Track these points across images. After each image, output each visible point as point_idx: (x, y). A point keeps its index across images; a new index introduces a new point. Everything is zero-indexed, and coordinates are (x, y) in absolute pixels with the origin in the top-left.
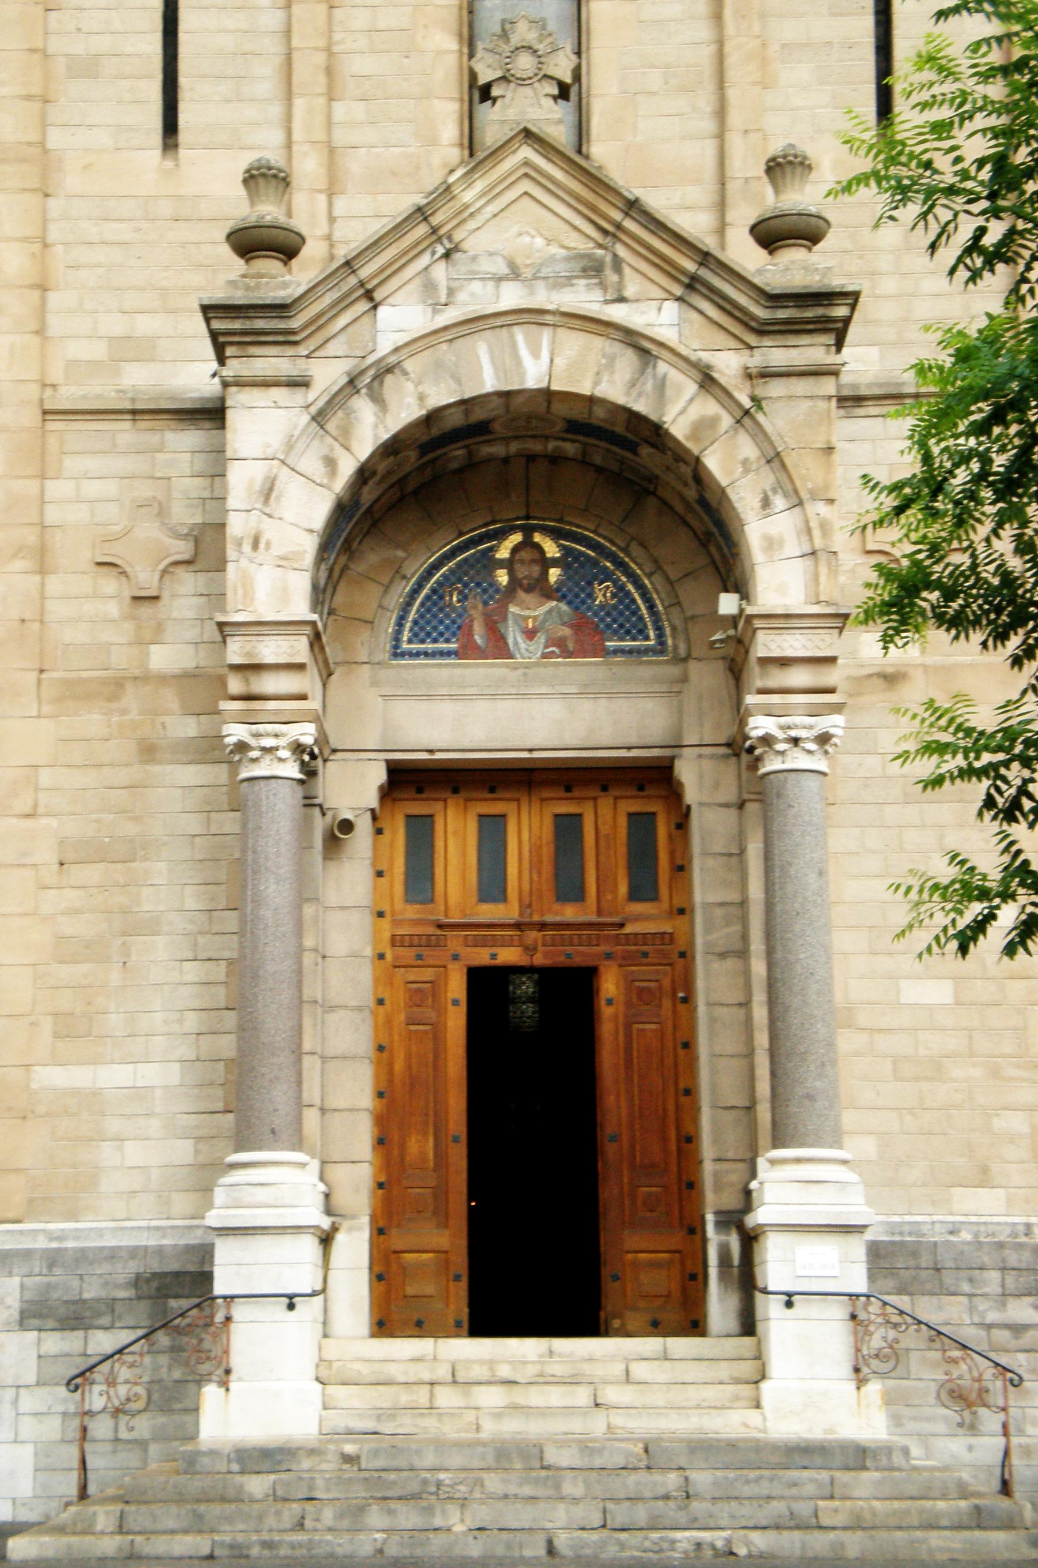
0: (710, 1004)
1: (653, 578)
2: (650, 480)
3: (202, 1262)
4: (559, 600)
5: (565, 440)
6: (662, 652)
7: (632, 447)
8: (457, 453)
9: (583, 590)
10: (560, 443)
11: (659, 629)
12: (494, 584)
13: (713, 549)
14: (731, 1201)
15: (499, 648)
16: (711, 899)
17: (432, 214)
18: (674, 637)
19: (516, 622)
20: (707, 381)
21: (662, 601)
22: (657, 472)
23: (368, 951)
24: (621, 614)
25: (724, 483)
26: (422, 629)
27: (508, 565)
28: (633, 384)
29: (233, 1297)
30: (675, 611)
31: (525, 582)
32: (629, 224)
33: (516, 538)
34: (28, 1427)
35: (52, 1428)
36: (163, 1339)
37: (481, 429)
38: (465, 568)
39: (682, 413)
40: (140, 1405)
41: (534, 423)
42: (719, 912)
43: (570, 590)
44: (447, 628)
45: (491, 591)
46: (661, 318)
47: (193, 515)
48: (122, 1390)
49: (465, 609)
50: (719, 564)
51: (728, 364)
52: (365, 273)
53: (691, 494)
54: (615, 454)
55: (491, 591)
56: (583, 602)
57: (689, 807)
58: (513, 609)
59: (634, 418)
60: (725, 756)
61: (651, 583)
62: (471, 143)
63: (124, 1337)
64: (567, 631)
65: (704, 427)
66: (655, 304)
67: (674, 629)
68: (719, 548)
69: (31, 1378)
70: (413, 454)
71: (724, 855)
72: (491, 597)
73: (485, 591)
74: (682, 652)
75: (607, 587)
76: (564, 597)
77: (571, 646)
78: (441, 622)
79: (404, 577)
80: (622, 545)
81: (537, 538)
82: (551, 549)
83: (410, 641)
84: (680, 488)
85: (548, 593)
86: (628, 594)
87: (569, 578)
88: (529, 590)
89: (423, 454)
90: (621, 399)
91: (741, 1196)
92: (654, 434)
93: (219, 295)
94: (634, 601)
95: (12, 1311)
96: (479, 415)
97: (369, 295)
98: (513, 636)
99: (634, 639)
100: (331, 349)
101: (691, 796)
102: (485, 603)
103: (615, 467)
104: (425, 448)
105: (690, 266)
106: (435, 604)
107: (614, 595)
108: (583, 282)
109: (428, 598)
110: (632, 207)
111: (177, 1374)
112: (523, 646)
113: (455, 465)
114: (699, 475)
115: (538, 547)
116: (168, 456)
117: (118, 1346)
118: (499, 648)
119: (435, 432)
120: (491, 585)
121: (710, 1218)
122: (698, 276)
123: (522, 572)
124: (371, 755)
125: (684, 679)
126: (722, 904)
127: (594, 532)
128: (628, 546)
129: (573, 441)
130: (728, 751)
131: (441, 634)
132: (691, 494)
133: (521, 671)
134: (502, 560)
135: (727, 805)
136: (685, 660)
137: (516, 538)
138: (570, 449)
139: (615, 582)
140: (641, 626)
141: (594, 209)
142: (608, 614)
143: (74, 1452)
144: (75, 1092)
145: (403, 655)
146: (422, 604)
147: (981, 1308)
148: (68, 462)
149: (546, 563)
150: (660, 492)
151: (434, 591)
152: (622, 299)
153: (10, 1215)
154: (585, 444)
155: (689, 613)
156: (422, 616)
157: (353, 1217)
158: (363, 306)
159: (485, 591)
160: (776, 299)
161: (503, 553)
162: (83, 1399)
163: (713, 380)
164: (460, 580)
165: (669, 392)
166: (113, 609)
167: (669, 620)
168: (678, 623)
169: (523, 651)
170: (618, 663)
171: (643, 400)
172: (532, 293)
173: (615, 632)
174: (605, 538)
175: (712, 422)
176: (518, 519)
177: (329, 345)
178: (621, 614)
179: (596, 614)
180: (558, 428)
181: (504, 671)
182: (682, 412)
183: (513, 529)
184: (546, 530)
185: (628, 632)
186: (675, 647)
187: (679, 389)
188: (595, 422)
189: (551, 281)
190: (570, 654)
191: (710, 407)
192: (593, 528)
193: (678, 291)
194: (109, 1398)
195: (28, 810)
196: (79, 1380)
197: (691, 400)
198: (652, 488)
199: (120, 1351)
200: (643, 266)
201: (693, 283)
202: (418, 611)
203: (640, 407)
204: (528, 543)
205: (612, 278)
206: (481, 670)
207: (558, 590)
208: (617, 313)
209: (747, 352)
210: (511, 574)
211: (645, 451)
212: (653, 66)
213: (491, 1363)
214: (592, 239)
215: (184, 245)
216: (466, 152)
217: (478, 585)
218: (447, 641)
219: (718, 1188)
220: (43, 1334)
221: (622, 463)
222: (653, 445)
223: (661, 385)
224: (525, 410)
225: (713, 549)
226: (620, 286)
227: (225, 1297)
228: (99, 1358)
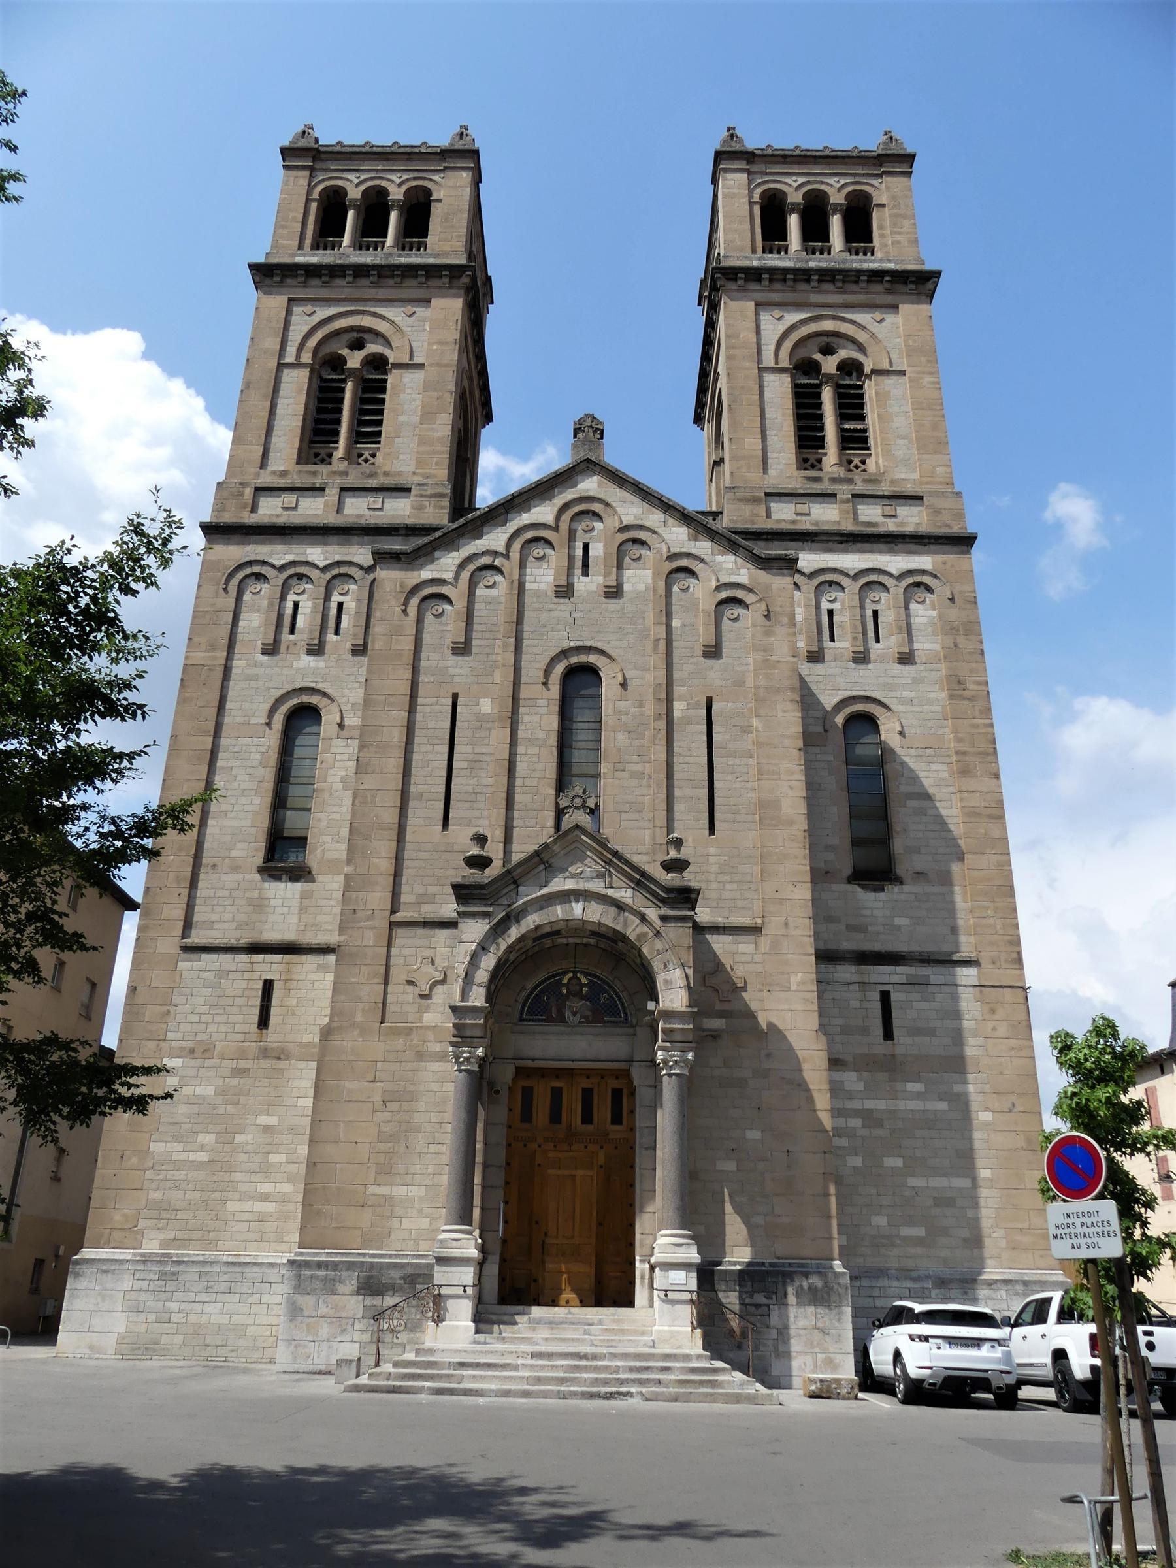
7: (616, 942)
8: (548, 942)
11: (625, 1014)
12: (561, 993)
14: (647, 1251)
20: (643, 918)
27: (567, 985)
28: (615, 919)
33: (571, 975)
35: (367, 1337)
37: (557, 933)
39: (633, 929)
40: (401, 1328)
46: (626, 894)
51: (652, 914)
52: (514, 874)
62: (557, 827)
64: (589, 1013)
69: (360, 1315)
74: (634, 1022)
82: (584, 980)
85: (582, 997)
90: (611, 925)
92: (624, 939)
93: (459, 880)
96: (556, 928)
100: (500, 901)
110: (616, 854)
114: (640, 954)
118: (562, 1019)
119: (539, 934)
121: (637, 1258)
122: (641, 880)
132: (638, 961)
138: (592, 941)
158: (512, 886)
161: (565, 981)
163: (646, 920)
175: (645, 935)
183: (569, 972)
184: (581, 972)
187: (633, 922)
191: (644, 929)
203: (618, 928)
204: (575, 977)
208: (610, 892)
211: (620, 944)
213: (366, 739)
226: (611, 882)
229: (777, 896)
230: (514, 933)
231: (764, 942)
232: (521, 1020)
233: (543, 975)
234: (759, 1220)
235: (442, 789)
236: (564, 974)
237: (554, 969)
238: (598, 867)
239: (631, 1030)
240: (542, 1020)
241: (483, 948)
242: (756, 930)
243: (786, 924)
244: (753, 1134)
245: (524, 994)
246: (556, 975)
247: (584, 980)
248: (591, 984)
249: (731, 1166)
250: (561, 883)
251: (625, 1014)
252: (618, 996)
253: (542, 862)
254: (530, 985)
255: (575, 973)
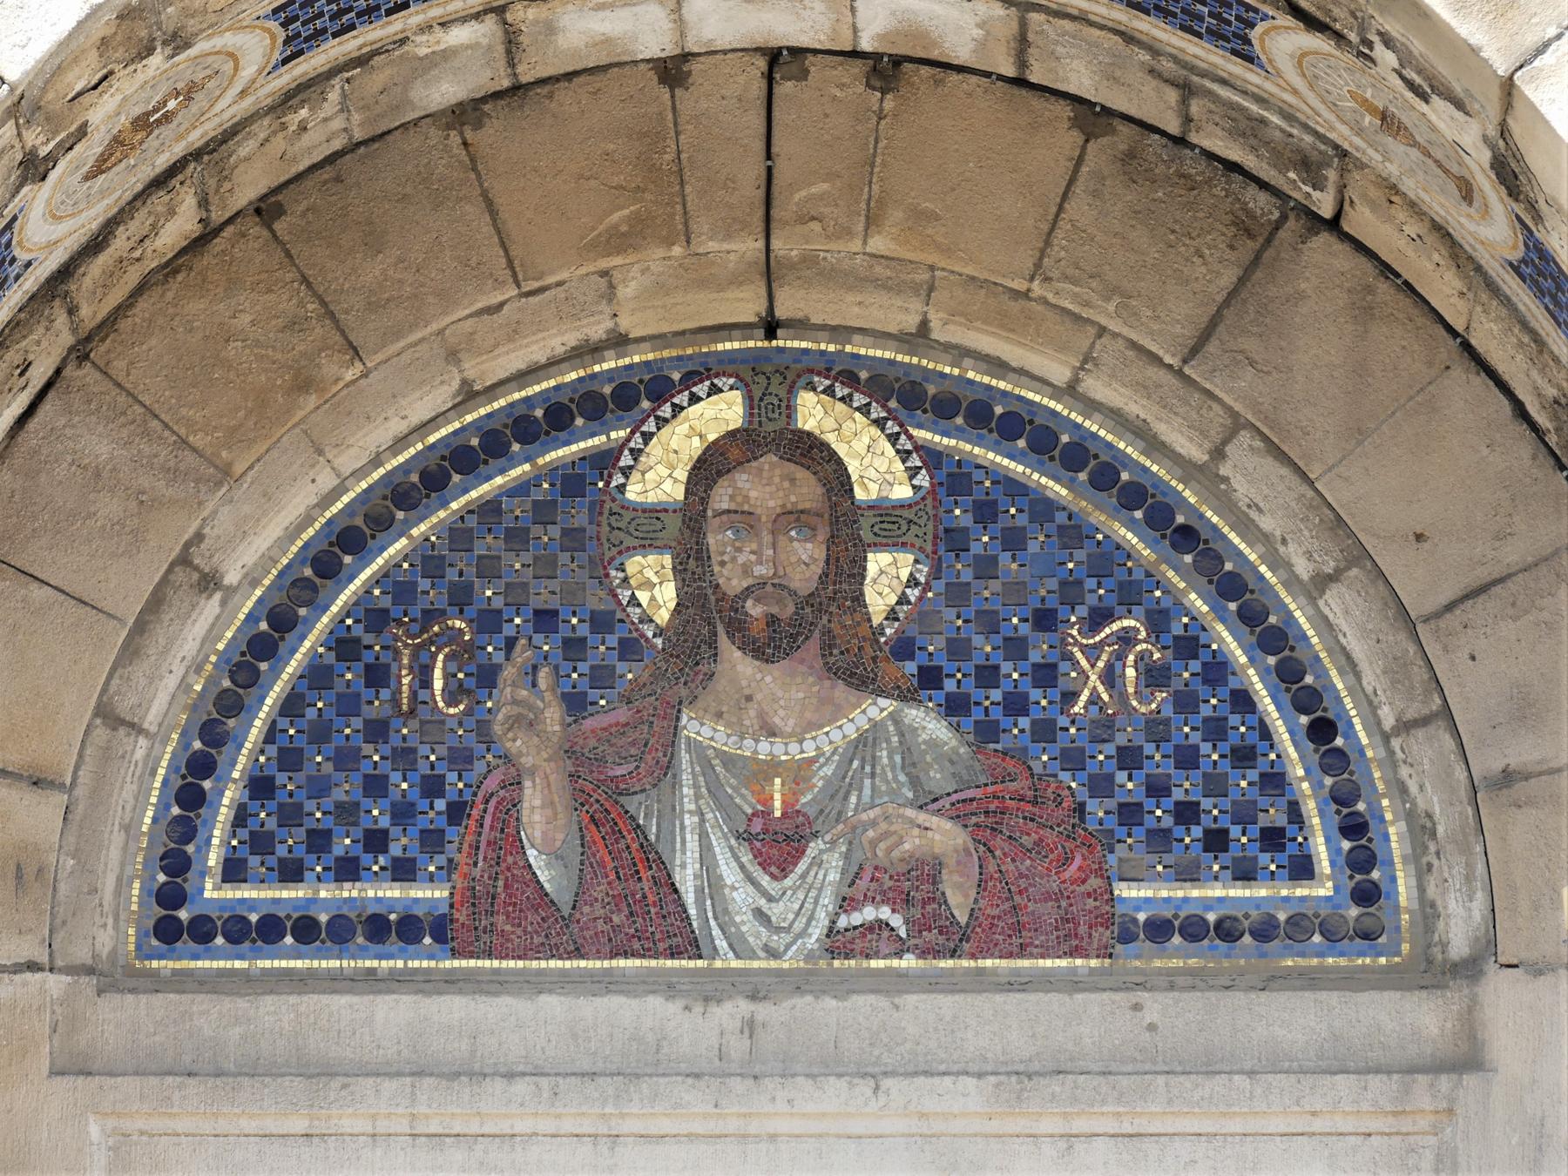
27: (686, 531)
33: (722, 412)
64: (944, 836)
74: (1459, 929)
85: (857, 663)
118: (640, 914)
132: (1491, 232)
161: (659, 479)
183: (701, 375)
184: (845, 377)
204: (770, 437)
232: (174, 923)
233: (396, 416)
236: (651, 394)
237: (528, 351)
239: (1423, 1018)
240: (404, 929)
245: (203, 633)
246: (558, 417)
247: (876, 467)
248: (958, 509)
251: (1362, 860)
252: (1273, 639)
254: (258, 540)
255: (770, 382)
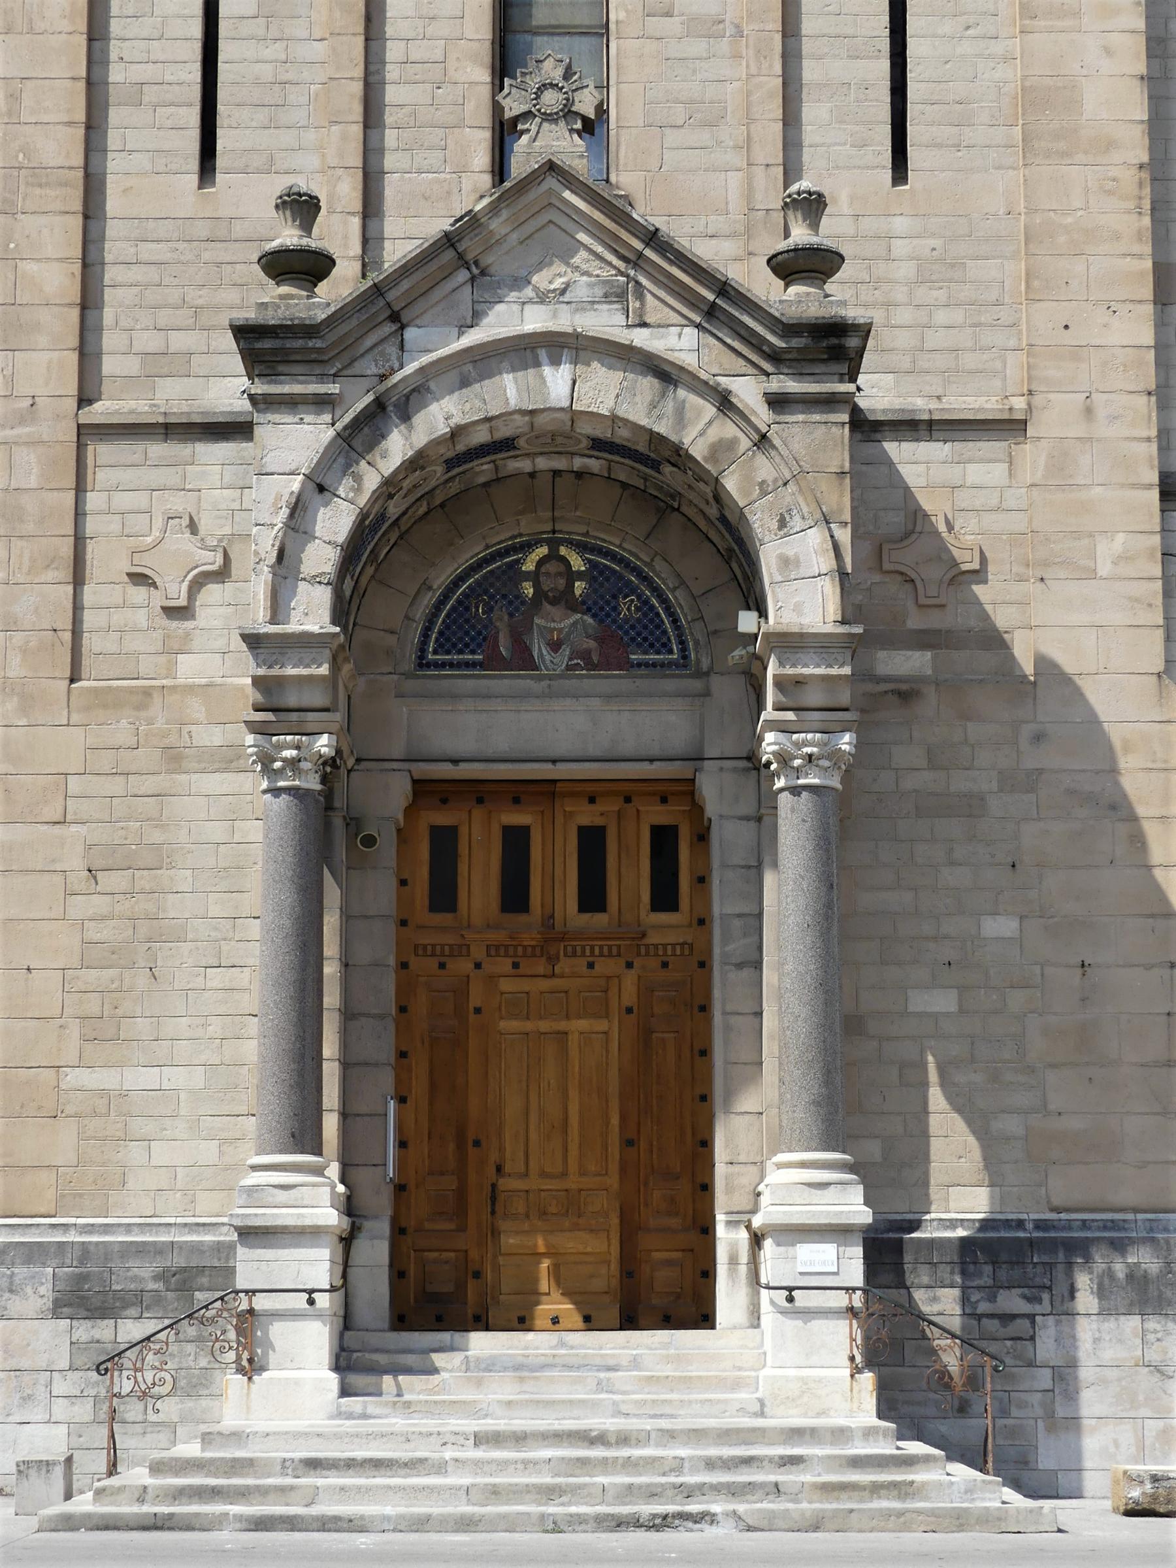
0: (725, 1013)
1: (677, 593)
2: (673, 497)
3: (227, 1259)
4: (583, 614)
5: (591, 457)
6: (685, 666)
7: (655, 465)
8: (483, 469)
9: (608, 603)
10: (587, 460)
13: (735, 566)
14: (745, 1203)
15: (524, 660)
16: (729, 910)
17: (458, 241)
18: (697, 652)
19: (541, 634)
21: (685, 616)
22: (679, 489)
23: (392, 961)
24: (645, 627)
25: (741, 504)
26: (448, 640)
27: (535, 577)
28: (653, 406)
29: (254, 1292)
30: (698, 625)
31: (550, 594)
32: (648, 253)
33: (543, 551)
34: (60, 1409)
35: (83, 1411)
36: (191, 1331)
37: (506, 445)
38: (492, 580)
39: (699, 431)
41: (559, 440)
42: (737, 923)
43: (595, 603)
44: (473, 639)
45: (517, 603)
46: (680, 342)
47: (222, 526)
48: (149, 1376)
49: (490, 620)
50: (741, 581)
52: (391, 296)
53: (713, 512)
54: (639, 471)
55: (517, 603)
56: (608, 615)
57: (710, 820)
58: (537, 621)
59: (655, 438)
60: (746, 770)
61: (676, 598)
62: (499, 169)
63: (150, 1326)
64: (592, 644)
65: (723, 448)
66: (677, 329)
67: (697, 643)
68: (741, 566)
69: (64, 1364)
70: (439, 469)
71: (743, 867)
72: (517, 609)
73: (510, 603)
74: (705, 664)
75: (632, 601)
76: (589, 609)
77: (595, 659)
78: (467, 633)
79: (430, 588)
80: (647, 560)
81: (563, 551)
83: (435, 652)
84: (703, 506)
86: (652, 607)
87: (595, 591)
88: (554, 602)
89: (449, 470)
90: (644, 422)
91: (751, 1197)
92: (678, 456)
93: (249, 315)
94: (658, 614)
95: (45, 1300)
96: (503, 432)
97: (395, 317)
98: (539, 648)
99: (658, 653)
101: (712, 809)
102: (511, 615)
103: (640, 483)
104: (450, 464)
105: (711, 297)
106: (461, 615)
107: (638, 609)
108: (605, 307)
109: (453, 609)
110: (652, 237)
111: (203, 1362)
112: (547, 657)
113: (482, 479)
114: (719, 496)
115: (564, 560)
116: (198, 468)
117: (145, 1336)
118: (524, 660)
119: (460, 447)
120: (517, 597)
121: (720, 1218)
122: (717, 304)
123: (547, 584)
124: (395, 765)
125: (707, 693)
126: (739, 916)
127: (620, 546)
128: (652, 560)
129: (597, 458)
130: (744, 764)
131: (467, 645)
132: (713, 512)
133: (545, 683)
134: (529, 572)
135: (747, 818)
136: (707, 674)
137: (543, 551)
138: (594, 465)
139: (639, 597)
140: (664, 640)
141: (617, 238)
142: (633, 627)
143: (105, 1431)
144: (103, 1092)
145: (428, 665)
146: (448, 616)
147: (973, 1299)
148: (101, 475)
149: (571, 576)
150: (684, 509)
151: (459, 602)
152: (644, 325)
153: (43, 1210)
154: (610, 461)
155: (711, 628)
156: (448, 627)
157: (376, 1217)
158: (389, 328)
159: (510, 603)
160: (789, 329)
161: (529, 566)
162: (112, 1382)
164: (486, 592)
165: (688, 414)
166: (141, 618)
167: (692, 634)
168: (702, 640)
169: (548, 662)
170: (642, 676)
171: (664, 421)
172: (555, 315)
173: (639, 645)
174: (630, 552)
176: (544, 533)
177: (356, 364)
178: (645, 627)
179: (620, 627)
180: (582, 446)
181: (529, 683)
182: (702, 433)
184: (570, 543)
185: (652, 645)
186: (698, 661)
187: (699, 413)
188: (618, 441)
189: (573, 305)
190: (595, 667)
191: (728, 429)
192: (618, 542)
193: (698, 319)
194: (136, 1381)
195: (58, 817)
196: (109, 1365)
197: (710, 423)
198: (676, 505)
199: (148, 1339)
200: (662, 294)
201: (711, 312)
202: (444, 621)
203: (661, 428)
205: (634, 304)
206: (506, 681)
207: (583, 603)
208: (640, 338)
209: (765, 378)
210: (537, 586)
211: (667, 469)
212: (677, 101)
214: (615, 267)
215: (219, 264)
216: (497, 178)
217: (504, 596)
218: (473, 652)
219: (729, 1190)
220: (75, 1323)
221: (646, 480)
222: (674, 465)
223: (680, 411)
224: (549, 428)
225: (735, 566)
226: (641, 312)
227: (246, 1292)
228: (127, 1345)
229: (1067, 338)
230: (398, 447)
231: (1032, 456)
234: (1011, 1125)
235: (194, 74)
238: (607, 273)
241: (319, 486)
242: (1011, 427)
243: (1089, 411)
244: (1000, 927)
249: (943, 1002)
250: (508, 319)
253: (462, 261)
254: (441, 578)
